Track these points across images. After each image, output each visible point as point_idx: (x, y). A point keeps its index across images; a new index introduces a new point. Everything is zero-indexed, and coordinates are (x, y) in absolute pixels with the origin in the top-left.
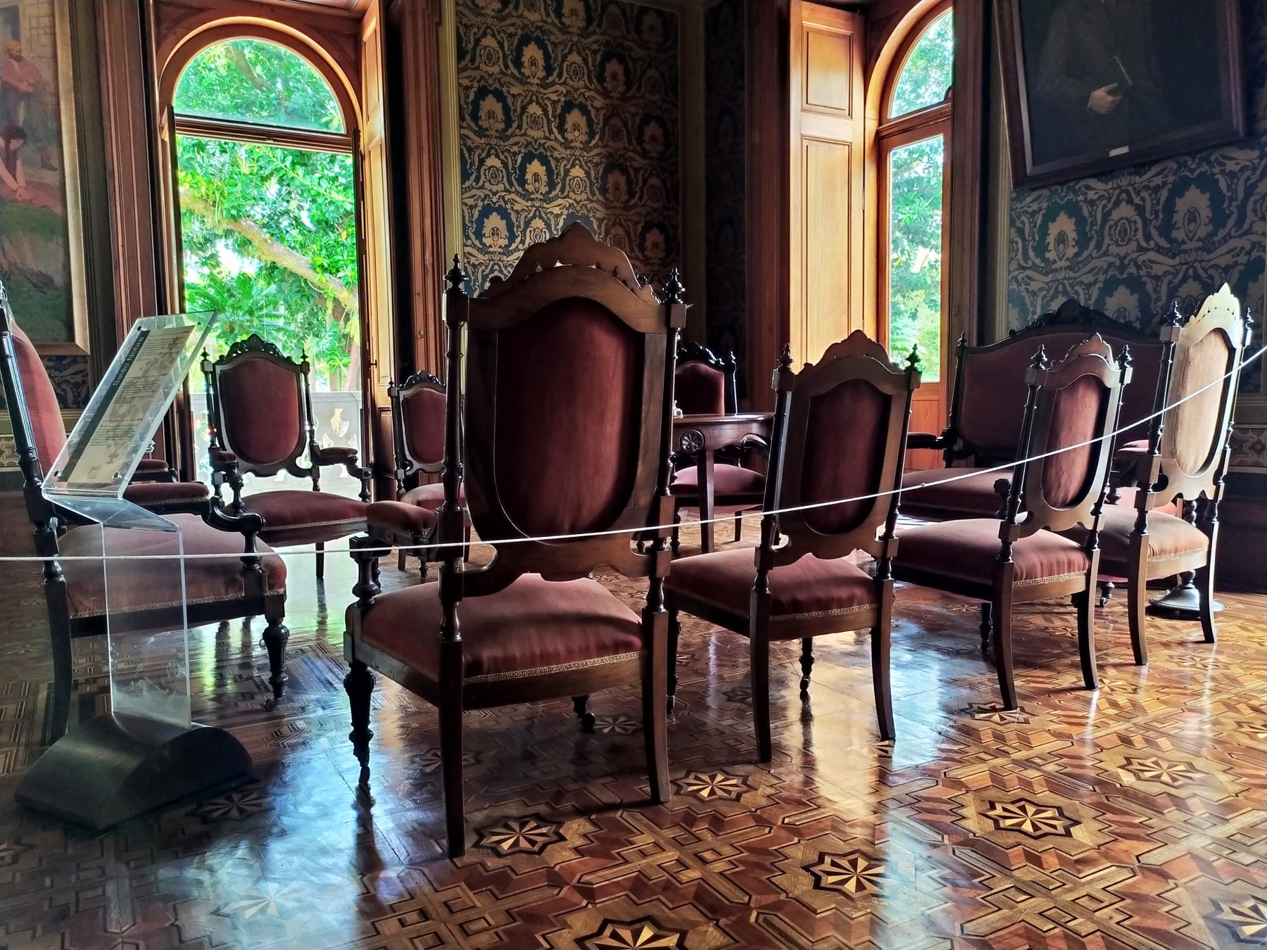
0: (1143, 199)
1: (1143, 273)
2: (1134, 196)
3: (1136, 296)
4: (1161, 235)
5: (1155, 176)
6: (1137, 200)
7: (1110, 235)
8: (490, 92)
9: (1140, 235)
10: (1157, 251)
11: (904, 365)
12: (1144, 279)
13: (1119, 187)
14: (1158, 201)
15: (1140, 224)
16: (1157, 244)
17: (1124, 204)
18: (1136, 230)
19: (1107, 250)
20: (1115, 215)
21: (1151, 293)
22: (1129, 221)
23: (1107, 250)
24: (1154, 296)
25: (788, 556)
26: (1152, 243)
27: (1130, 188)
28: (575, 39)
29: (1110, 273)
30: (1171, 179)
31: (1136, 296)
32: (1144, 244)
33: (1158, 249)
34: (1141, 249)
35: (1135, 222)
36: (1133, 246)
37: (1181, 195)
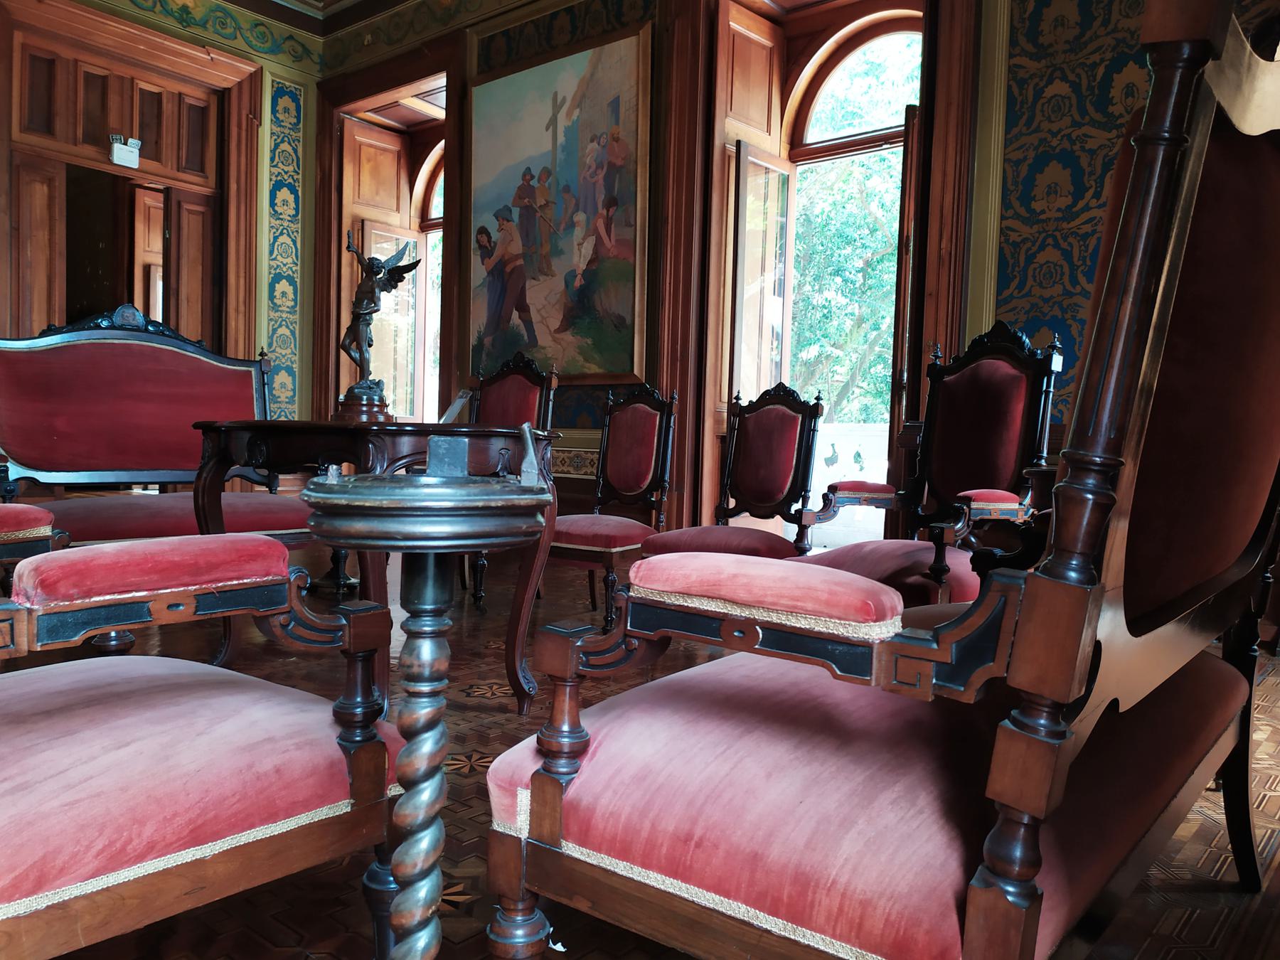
0: (1078, 76)
1: (1076, 147)
2: (1061, 242)
3: (1068, 172)
4: (1097, 111)
5: (1092, 53)
6: (1072, 77)
7: (1042, 111)
8: (287, 93)
9: (1066, 279)
10: (1093, 126)
11: (813, 402)
12: (1070, 322)
13: (1045, 231)
14: (1094, 77)
15: (1066, 269)
16: (1092, 119)
17: (1057, 81)
18: (1063, 274)
19: (1039, 126)
20: (1041, 258)
21: (1076, 335)
22: (1056, 265)
23: (1039, 126)
24: (1088, 170)
25: (736, 512)
26: (1078, 289)
27: (1064, 66)
28: (286, 224)
29: (1041, 149)
30: (1109, 55)
31: (1068, 172)
32: (1069, 287)
33: (1093, 123)
34: (1076, 124)
35: (1061, 266)
36: (1067, 120)
37: (1119, 72)
